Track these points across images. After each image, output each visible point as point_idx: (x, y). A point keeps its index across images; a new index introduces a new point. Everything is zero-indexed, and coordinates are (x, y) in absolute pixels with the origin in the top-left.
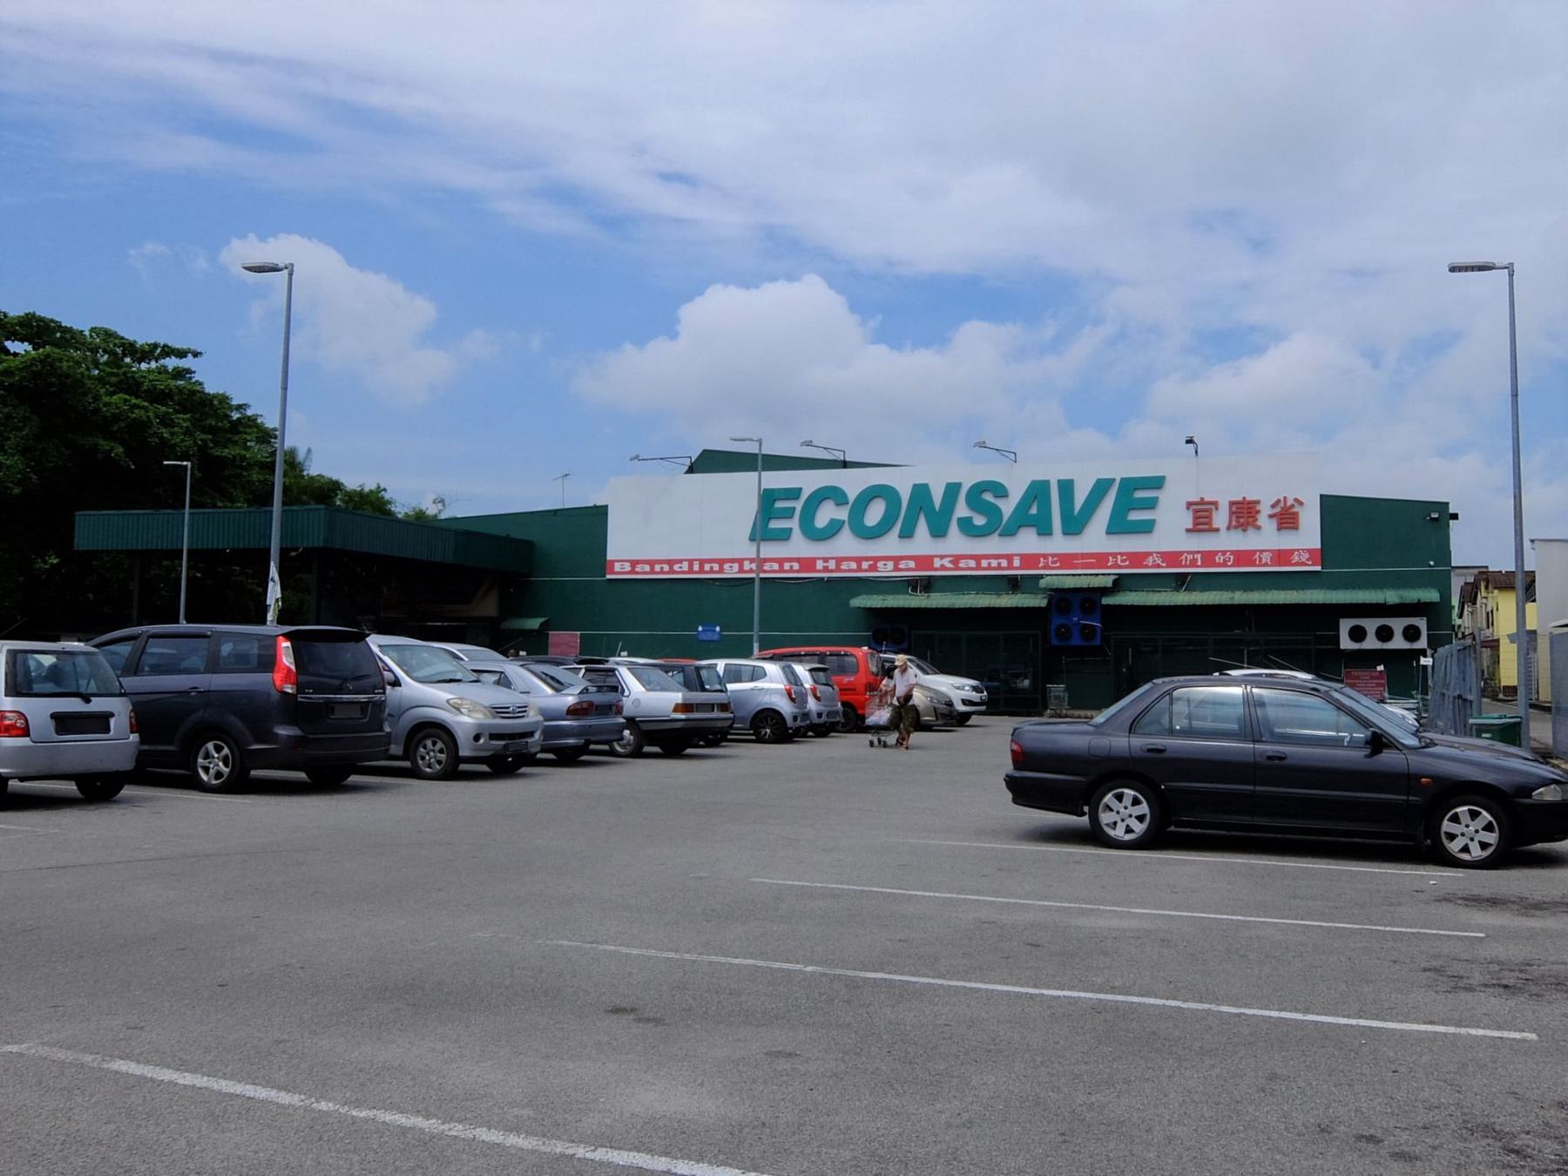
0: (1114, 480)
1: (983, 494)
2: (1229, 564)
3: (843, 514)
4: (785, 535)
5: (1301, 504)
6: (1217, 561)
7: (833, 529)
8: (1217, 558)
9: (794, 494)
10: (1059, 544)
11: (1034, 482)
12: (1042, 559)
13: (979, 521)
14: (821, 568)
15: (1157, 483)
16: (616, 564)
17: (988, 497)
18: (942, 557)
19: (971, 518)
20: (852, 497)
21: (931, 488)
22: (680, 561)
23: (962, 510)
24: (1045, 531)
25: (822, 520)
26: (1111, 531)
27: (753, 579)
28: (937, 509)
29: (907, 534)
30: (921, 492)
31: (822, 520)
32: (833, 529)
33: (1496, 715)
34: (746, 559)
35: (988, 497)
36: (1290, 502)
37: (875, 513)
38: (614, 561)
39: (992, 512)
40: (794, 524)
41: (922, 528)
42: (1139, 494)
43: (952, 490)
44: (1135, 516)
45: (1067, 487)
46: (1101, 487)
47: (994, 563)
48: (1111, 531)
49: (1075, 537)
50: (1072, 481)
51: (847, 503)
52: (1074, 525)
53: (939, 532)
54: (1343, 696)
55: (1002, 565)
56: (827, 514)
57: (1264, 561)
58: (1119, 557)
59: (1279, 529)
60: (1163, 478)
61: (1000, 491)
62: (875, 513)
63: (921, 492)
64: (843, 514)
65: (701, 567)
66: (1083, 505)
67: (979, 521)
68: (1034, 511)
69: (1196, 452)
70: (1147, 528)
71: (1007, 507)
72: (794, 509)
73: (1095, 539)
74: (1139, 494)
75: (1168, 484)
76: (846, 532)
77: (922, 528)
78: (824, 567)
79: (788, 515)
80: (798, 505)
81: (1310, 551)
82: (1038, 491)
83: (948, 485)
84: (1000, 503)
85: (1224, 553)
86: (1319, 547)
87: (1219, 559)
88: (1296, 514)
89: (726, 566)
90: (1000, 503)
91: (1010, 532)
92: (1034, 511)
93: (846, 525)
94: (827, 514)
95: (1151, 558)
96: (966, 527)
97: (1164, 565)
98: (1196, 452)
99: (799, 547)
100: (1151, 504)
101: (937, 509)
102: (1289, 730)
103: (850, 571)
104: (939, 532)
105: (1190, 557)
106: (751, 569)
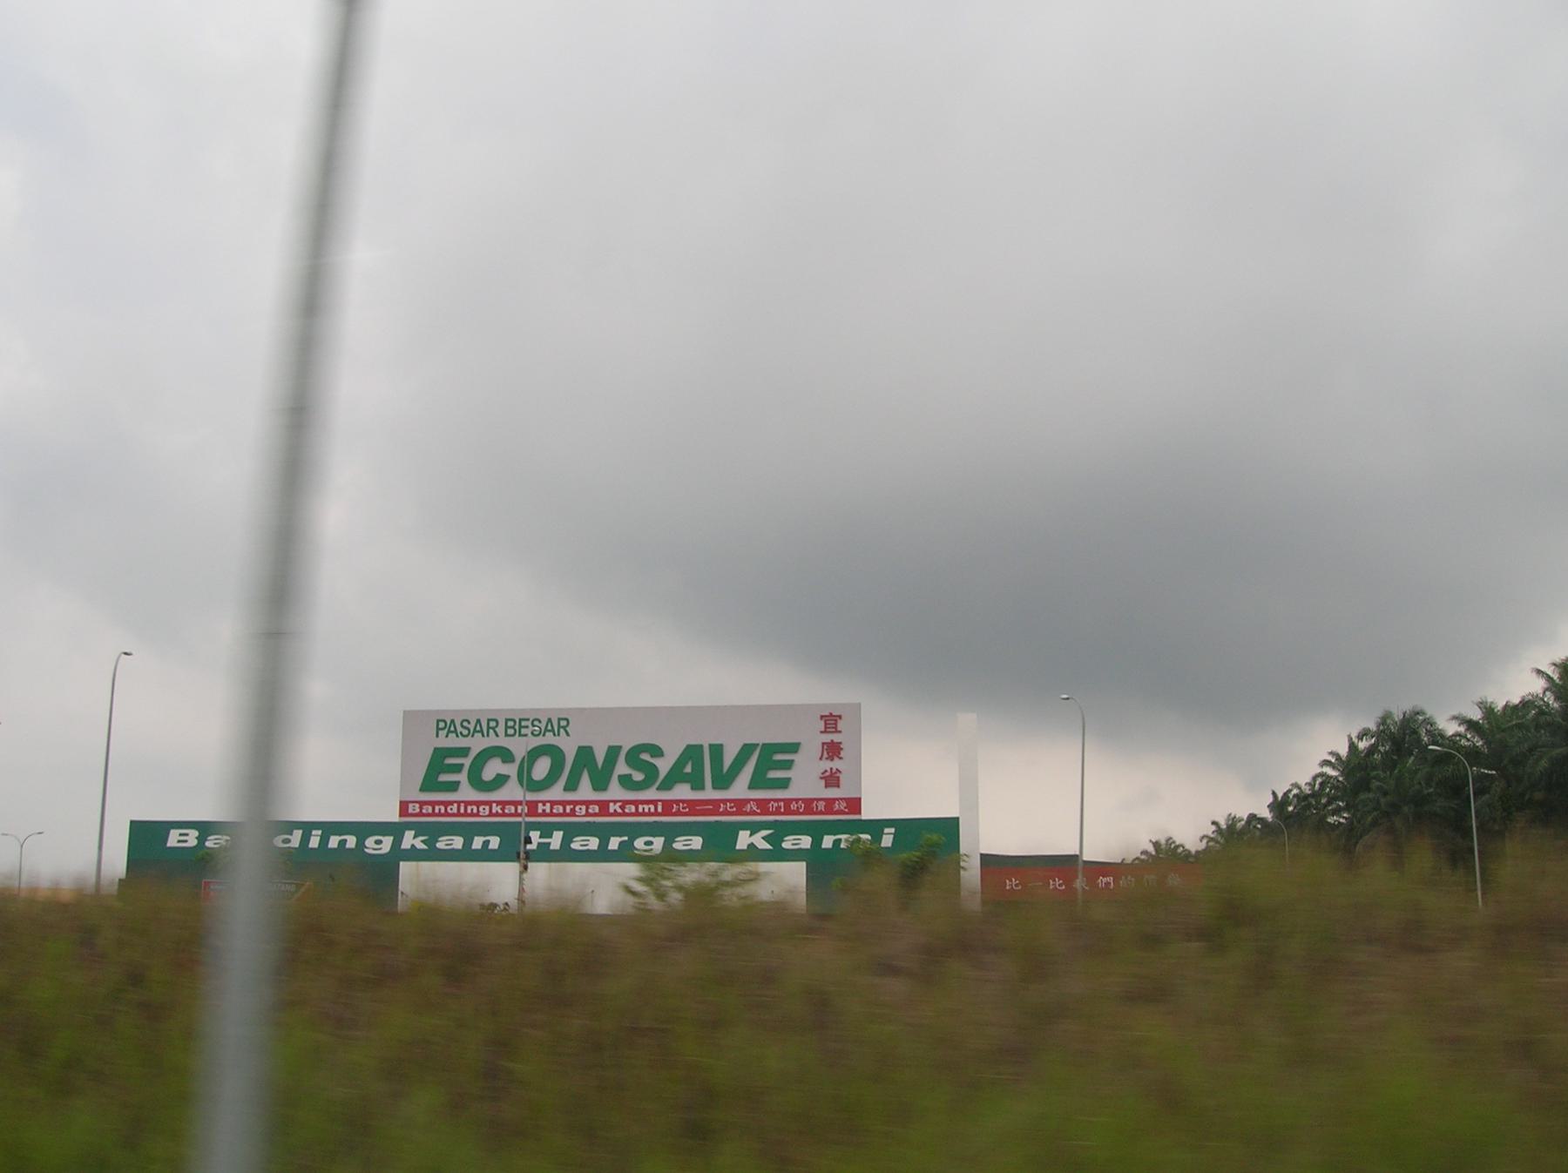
2: (801, 811)
3: (511, 770)
4: (454, 787)
5: (840, 772)
6: (792, 808)
7: (501, 780)
8: (792, 806)
9: (464, 752)
10: (710, 794)
11: (689, 747)
12: (675, 806)
13: (638, 777)
15: (794, 748)
16: (411, 805)
17: (645, 757)
18: (615, 802)
22: (451, 803)
23: (622, 768)
24: (698, 785)
25: (489, 773)
26: (751, 787)
27: (520, 823)
29: (572, 786)
30: (585, 753)
31: (489, 773)
32: (501, 780)
34: (494, 802)
35: (645, 757)
36: (834, 770)
37: (542, 768)
39: (651, 772)
40: (462, 777)
41: (585, 781)
43: (613, 752)
45: (717, 750)
46: (747, 750)
48: (751, 787)
50: (721, 746)
52: (723, 781)
53: (600, 784)
56: (492, 769)
57: (819, 809)
58: (681, 805)
59: (826, 787)
61: (657, 751)
62: (542, 768)
63: (585, 753)
64: (511, 770)
67: (638, 777)
68: (688, 769)
69: (40, 833)
70: (784, 784)
71: (664, 766)
72: (462, 765)
75: (802, 750)
77: (585, 781)
79: (458, 769)
80: (467, 762)
82: (692, 753)
83: (610, 748)
84: (657, 762)
85: (797, 800)
87: (793, 806)
88: (838, 777)
89: (370, 842)
90: (657, 762)
91: (667, 785)
92: (688, 769)
94: (492, 769)
95: (749, 805)
96: (626, 782)
97: (759, 811)
98: (40, 833)
99: (467, 793)
103: (650, 814)
104: (600, 784)
105: (776, 805)
106: (751, 845)
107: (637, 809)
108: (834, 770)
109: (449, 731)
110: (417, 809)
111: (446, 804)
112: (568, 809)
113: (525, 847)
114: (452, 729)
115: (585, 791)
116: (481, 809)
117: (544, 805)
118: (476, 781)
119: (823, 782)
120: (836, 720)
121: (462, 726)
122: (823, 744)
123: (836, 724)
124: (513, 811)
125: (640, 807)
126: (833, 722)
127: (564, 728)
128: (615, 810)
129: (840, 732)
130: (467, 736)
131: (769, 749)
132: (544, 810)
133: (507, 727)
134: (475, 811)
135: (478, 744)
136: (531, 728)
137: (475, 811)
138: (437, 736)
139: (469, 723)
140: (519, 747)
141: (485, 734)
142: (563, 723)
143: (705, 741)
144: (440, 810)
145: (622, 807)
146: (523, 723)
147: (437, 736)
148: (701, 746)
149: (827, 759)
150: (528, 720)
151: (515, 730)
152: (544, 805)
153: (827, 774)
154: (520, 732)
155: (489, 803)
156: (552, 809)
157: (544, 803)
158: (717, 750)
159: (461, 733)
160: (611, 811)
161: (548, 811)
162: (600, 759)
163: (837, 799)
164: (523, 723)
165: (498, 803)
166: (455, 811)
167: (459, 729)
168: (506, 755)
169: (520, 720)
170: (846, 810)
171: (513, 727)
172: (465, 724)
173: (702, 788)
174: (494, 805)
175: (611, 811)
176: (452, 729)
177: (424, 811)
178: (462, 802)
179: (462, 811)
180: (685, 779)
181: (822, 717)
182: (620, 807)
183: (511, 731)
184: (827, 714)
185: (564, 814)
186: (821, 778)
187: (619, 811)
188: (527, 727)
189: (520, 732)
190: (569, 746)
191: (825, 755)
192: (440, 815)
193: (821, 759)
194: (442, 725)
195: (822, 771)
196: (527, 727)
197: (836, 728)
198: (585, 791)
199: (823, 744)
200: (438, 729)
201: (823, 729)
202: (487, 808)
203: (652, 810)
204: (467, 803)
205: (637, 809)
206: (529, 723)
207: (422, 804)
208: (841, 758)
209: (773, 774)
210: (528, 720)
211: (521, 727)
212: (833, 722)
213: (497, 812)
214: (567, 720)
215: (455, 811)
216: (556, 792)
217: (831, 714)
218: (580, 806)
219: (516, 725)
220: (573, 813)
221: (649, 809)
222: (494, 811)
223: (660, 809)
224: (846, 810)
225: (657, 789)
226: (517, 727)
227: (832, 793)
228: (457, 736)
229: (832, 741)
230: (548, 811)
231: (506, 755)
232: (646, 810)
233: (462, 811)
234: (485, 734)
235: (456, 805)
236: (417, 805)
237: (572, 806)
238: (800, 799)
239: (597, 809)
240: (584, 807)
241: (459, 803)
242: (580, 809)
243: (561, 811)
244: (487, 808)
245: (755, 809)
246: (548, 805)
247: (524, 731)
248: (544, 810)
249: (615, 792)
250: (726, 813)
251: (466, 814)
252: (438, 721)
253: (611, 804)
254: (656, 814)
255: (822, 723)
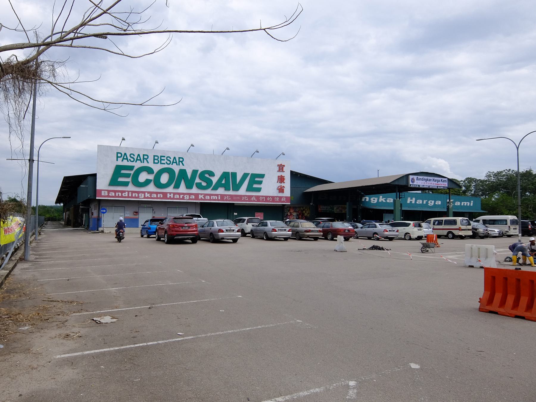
0: (249, 173)
1: (206, 175)
4: (126, 184)
7: (147, 182)
9: (131, 168)
10: (231, 193)
14: (126, 192)
15: (262, 176)
16: (103, 192)
17: (207, 176)
19: (201, 183)
20: (155, 172)
21: (263, 182)
22: (125, 192)
23: (198, 180)
24: (227, 189)
28: (189, 179)
29: (177, 186)
30: (183, 172)
32: (147, 182)
33: (200, 221)
35: (207, 176)
36: (282, 186)
38: (101, 190)
39: (209, 182)
41: (183, 184)
42: (257, 179)
43: (195, 172)
44: (255, 186)
45: (234, 175)
46: (245, 176)
47: (214, 197)
49: (128, 178)
50: (236, 173)
51: (153, 173)
52: (237, 187)
53: (189, 187)
54: (90, 221)
55: (169, 194)
57: (277, 200)
60: (264, 175)
61: (212, 174)
62: (164, 178)
64: (151, 177)
65: (132, 195)
66: (308, 192)
67: (204, 184)
68: (223, 182)
70: (259, 190)
71: (215, 180)
73: (243, 191)
74: (257, 179)
76: (152, 184)
77: (183, 184)
78: (171, 195)
79: (127, 176)
80: (132, 172)
81: (286, 197)
82: (225, 175)
84: (211, 178)
85: (269, 197)
86: (290, 196)
87: (268, 199)
88: (283, 189)
90: (211, 178)
91: (215, 188)
92: (223, 182)
93: (153, 181)
94: (143, 177)
96: (199, 186)
100: (260, 183)
101: (189, 179)
102: (57, 229)
103: (215, 200)
107: (115, 194)
108: (282, 186)
109: (123, 159)
110: (172, 195)
111: (122, 192)
112: (181, 196)
113: (102, 208)
114: (125, 157)
115: (182, 189)
116: (140, 195)
117: (170, 194)
118: (158, 184)
119: (278, 190)
120: (283, 167)
121: (131, 157)
122: (278, 176)
123: (283, 169)
124: (209, 198)
125: (212, 197)
126: (282, 168)
127: (182, 162)
128: (148, 196)
129: (284, 171)
130: (133, 161)
131: (254, 176)
132: (170, 197)
133: (154, 159)
134: (137, 196)
135: (138, 165)
136: (166, 161)
137: (137, 196)
138: (117, 160)
139: (170, 158)
140: (156, 168)
141: (178, 164)
142: (181, 160)
143: (230, 170)
144: (119, 194)
145: (204, 197)
146: (162, 158)
147: (117, 160)
148: (229, 172)
149: (279, 182)
150: (164, 157)
151: (158, 161)
152: (170, 194)
153: (280, 187)
154: (161, 161)
155: (144, 193)
156: (174, 196)
157: (170, 193)
158: (234, 175)
159: (130, 160)
160: (200, 198)
161: (172, 197)
162: (189, 175)
163: (283, 197)
164: (162, 158)
165: (148, 192)
166: (127, 195)
167: (129, 158)
168: (149, 171)
169: (161, 156)
170: (286, 201)
171: (157, 159)
172: (132, 156)
173: (229, 190)
174: (146, 193)
175: (200, 198)
176: (125, 157)
177: (175, 197)
178: (130, 191)
179: (130, 195)
180: (222, 186)
181: (284, 166)
182: (150, 195)
183: (156, 161)
184: (280, 164)
185: (180, 199)
186: (277, 189)
187: (203, 198)
188: (164, 160)
189: (161, 161)
190: (176, 168)
191: (279, 181)
192: (119, 197)
193: (277, 182)
194: (119, 155)
195: (278, 186)
196: (164, 160)
197: (283, 170)
198: (182, 189)
199: (278, 176)
200: (117, 157)
201: (278, 170)
202: (143, 195)
203: (216, 198)
204: (133, 192)
205: (115, 194)
206: (165, 158)
207: (109, 191)
208: (284, 183)
209: (120, 179)
210: (164, 157)
211: (161, 160)
212: (282, 168)
213: (201, 198)
214: (183, 158)
215: (127, 195)
216: (170, 189)
217: (281, 164)
218: (186, 196)
219: (158, 159)
220: (183, 198)
221: (467, 204)
222: (146, 196)
223: (219, 198)
224: (286, 201)
225: (211, 190)
226: (159, 159)
227: (280, 195)
228: (128, 161)
229: (281, 175)
230: (172, 197)
231: (149, 171)
232: (214, 198)
233: (130, 195)
234: (178, 164)
235: (127, 193)
236: (106, 192)
237: (183, 195)
238: (270, 196)
239: (193, 197)
240: (188, 196)
241: (128, 192)
242: (187, 197)
243: (209, 198)
244: (143, 195)
245: (255, 199)
246: (172, 194)
247: (163, 162)
248: (170, 197)
249: (195, 190)
250: (244, 201)
251: (132, 197)
252: (118, 153)
253: (200, 195)
254: (218, 200)
255: (278, 168)
